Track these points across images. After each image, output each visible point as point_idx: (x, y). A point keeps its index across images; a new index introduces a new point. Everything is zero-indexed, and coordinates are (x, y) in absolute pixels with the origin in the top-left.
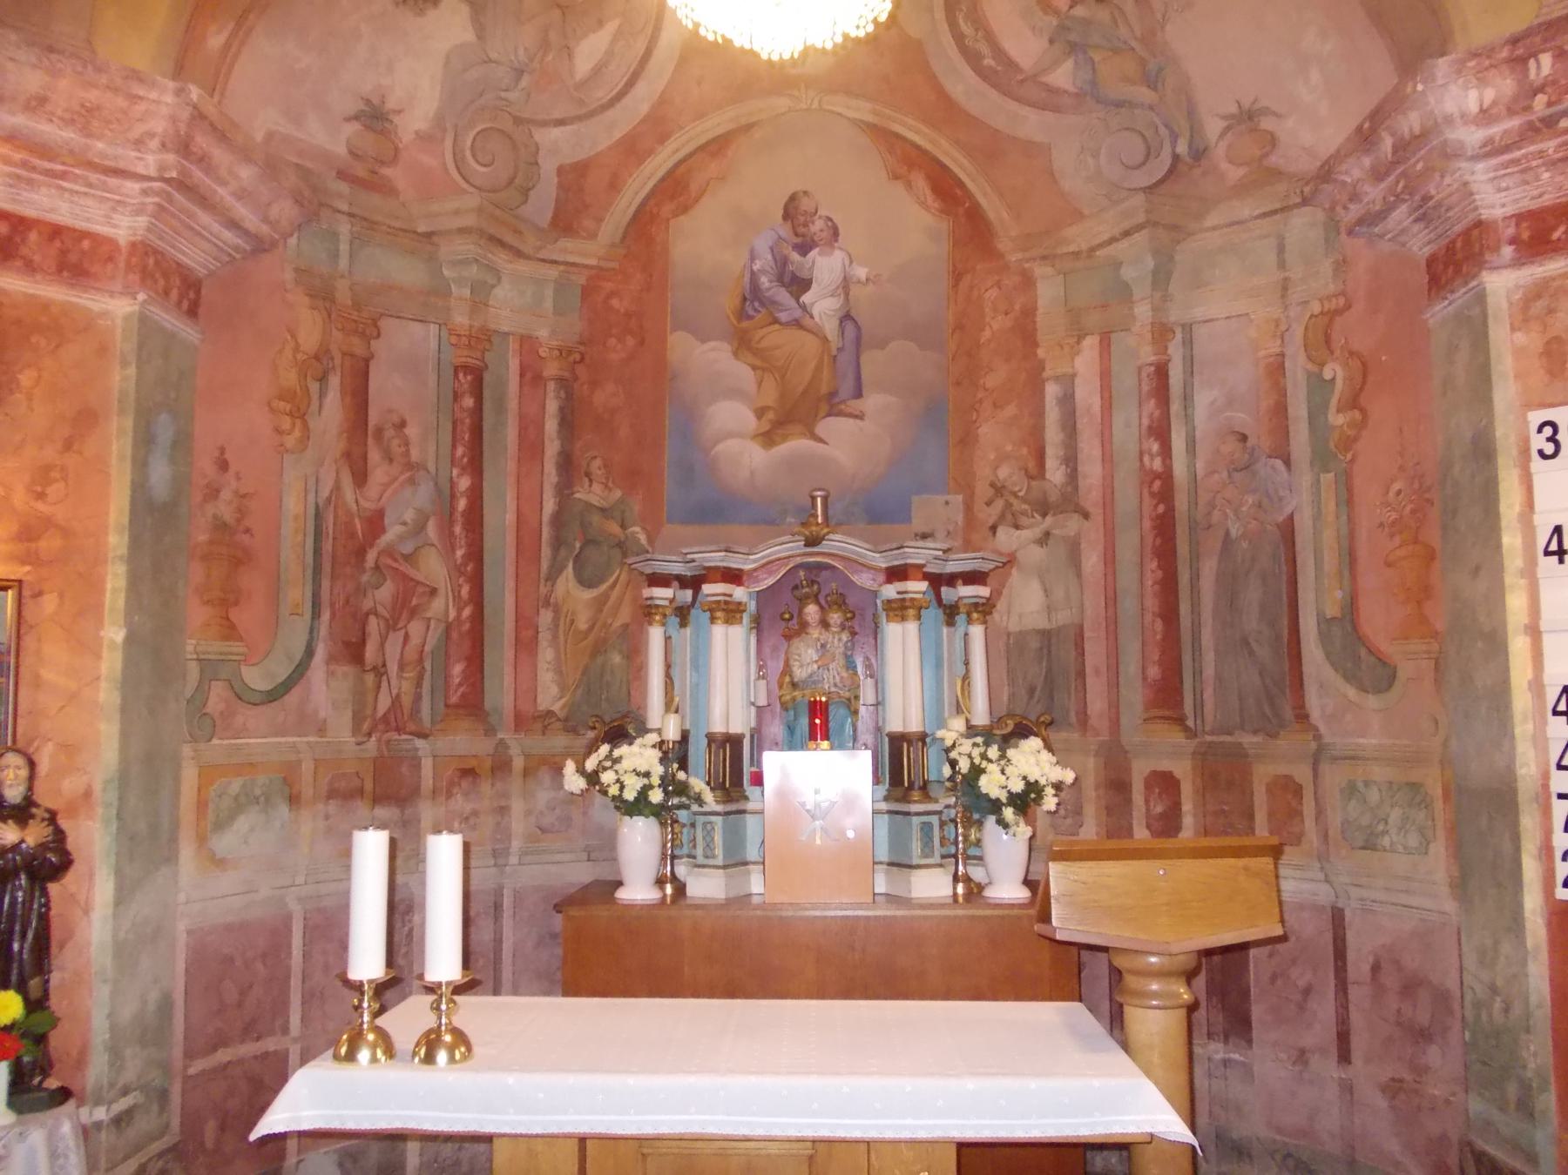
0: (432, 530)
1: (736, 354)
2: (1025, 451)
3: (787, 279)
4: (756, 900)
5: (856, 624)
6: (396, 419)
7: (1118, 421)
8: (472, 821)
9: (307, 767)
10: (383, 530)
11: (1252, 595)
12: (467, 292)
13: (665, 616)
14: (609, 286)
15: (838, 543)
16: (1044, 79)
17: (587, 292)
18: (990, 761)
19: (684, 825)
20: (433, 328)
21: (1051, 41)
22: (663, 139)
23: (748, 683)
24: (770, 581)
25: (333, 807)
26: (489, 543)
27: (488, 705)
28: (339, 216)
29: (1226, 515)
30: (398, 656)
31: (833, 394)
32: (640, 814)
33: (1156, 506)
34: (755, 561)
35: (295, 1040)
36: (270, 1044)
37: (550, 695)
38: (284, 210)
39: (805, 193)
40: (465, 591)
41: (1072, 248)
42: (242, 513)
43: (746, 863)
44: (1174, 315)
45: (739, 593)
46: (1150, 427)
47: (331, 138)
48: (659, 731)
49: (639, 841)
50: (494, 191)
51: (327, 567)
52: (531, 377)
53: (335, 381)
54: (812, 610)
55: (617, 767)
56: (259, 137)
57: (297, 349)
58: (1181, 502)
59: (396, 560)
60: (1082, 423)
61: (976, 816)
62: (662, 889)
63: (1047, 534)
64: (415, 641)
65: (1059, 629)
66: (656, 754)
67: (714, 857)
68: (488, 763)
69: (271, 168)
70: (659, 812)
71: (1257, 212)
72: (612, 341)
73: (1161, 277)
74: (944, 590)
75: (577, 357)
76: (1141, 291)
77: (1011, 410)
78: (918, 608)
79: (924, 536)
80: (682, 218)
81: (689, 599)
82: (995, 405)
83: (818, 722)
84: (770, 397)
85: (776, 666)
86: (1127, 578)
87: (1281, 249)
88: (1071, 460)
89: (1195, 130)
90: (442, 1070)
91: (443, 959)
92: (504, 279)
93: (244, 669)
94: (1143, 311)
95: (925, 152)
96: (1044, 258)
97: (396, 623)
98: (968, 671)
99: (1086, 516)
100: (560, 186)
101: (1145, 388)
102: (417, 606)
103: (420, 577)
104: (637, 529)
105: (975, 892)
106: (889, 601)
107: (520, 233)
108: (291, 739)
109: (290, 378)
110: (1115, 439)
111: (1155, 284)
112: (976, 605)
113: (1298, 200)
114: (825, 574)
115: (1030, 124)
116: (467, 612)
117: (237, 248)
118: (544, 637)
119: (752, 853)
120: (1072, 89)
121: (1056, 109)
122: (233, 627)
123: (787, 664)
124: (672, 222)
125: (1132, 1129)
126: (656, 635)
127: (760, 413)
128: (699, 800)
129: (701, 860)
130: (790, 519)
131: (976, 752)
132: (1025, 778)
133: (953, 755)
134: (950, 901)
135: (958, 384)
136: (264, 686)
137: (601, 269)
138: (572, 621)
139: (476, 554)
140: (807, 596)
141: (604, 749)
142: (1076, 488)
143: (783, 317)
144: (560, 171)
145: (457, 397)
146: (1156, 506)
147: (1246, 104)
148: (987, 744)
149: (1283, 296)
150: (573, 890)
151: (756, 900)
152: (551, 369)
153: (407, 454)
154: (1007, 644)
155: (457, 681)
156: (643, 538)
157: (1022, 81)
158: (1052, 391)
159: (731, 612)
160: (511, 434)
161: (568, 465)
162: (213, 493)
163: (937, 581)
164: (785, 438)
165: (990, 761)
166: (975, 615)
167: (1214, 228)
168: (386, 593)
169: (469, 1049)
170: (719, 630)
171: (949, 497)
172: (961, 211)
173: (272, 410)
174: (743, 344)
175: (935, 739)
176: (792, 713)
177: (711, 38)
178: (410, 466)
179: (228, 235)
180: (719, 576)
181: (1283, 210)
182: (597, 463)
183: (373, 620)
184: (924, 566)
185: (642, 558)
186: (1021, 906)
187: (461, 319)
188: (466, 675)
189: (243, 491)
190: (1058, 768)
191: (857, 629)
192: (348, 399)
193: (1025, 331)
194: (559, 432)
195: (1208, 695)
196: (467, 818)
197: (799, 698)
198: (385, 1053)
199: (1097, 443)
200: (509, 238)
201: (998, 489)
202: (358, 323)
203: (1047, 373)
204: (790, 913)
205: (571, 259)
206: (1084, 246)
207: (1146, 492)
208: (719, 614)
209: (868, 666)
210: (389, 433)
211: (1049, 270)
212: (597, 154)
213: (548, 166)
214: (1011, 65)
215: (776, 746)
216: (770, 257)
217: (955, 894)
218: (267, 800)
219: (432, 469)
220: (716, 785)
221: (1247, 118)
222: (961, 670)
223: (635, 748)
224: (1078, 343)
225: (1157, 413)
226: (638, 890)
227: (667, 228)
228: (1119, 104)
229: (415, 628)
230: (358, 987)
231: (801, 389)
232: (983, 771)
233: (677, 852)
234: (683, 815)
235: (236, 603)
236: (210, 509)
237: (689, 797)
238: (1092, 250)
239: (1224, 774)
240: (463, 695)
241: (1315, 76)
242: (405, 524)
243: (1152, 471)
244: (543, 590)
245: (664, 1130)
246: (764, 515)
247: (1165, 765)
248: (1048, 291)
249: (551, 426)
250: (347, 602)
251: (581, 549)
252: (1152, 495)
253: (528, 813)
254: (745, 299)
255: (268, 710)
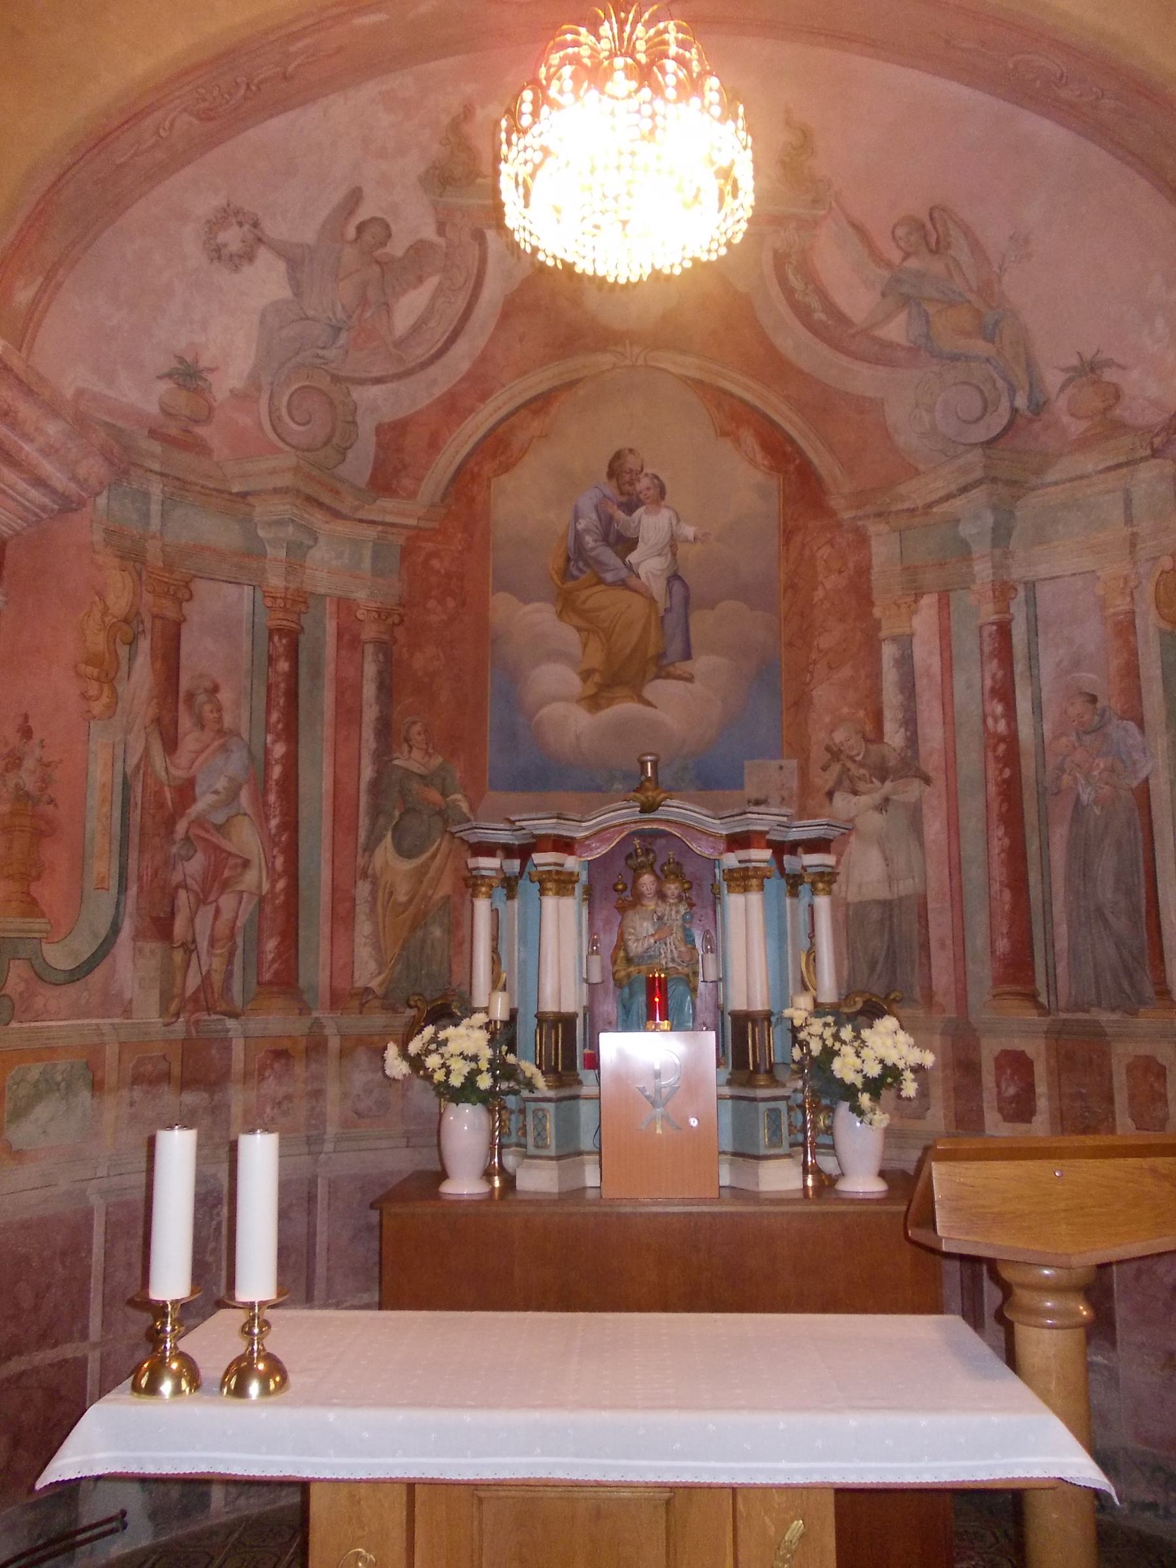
0: (244, 797)
1: (560, 615)
2: (861, 713)
3: (612, 538)
4: (591, 1194)
5: (693, 894)
6: (208, 684)
7: (959, 681)
8: (284, 1107)
9: (111, 1052)
10: (194, 800)
11: (1106, 864)
12: (282, 554)
13: (491, 887)
14: (429, 546)
15: (678, 810)
16: (877, 333)
17: (406, 553)
18: (844, 1042)
19: (512, 1112)
20: (248, 590)
21: (883, 295)
22: (484, 397)
23: (580, 957)
24: (604, 850)
25: (138, 1093)
26: (305, 812)
27: (302, 983)
28: (151, 476)
29: (1075, 779)
30: (208, 933)
31: (661, 655)
32: (467, 1101)
33: (1001, 771)
34: (587, 828)
35: (94, 1346)
36: (69, 1351)
37: (367, 971)
38: (93, 468)
39: (631, 451)
40: (279, 862)
41: (907, 505)
42: (45, 782)
43: (580, 1153)
44: (1017, 573)
45: (571, 863)
46: (993, 691)
47: (142, 396)
48: (486, 1010)
49: (466, 1127)
50: (308, 450)
51: (135, 837)
52: (349, 640)
53: (144, 644)
54: (647, 881)
55: (442, 1050)
56: (69, 394)
57: (105, 611)
58: (1028, 767)
59: (207, 831)
60: (921, 683)
61: (825, 1102)
62: (490, 1182)
63: (887, 800)
64: (226, 915)
65: (901, 899)
66: (482, 1037)
67: (546, 1147)
68: (302, 1045)
69: (81, 424)
70: (488, 1099)
71: (1100, 467)
72: (432, 604)
73: (1001, 535)
74: (786, 858)
75: (396, 619)
76: (981, 548)
77: (846, 672)
78: (762, 876)
79: (758, 803)
80: (504, 477)
81: (517, 869)
82: (830, 668)
83: (654, 999)
84: (595, 658)
85: (609, 940)
86: (972, 847)
87: (1128, 503)
88: (910, 722)
89: (1034, 383)
90: (254, 1404)
91: (257, 1277)
92: (322, 540)
93: (45, 947)
94: (983, 570)
95: (754, 409)
96: (879, 515)
97: (206, 898)
98: (813, 944)
99: (927, 780)
100: (379, 445)
101: (987, 649)
102: (229, 878)
103: (233, 850)
104: (458, 796)
105: (826, 1184)
106: (730, 871)
107: (337, 493)
108: (94, 1021)
109: (98, 642)
110: (957, 700)
111: (995, 543)
112: (822, 874)
113: (1149, 452)
114: (661, 842)
115: (864, 379)
116: (281, 884)
117: (43, 508)
118: (362, 910)
119: (587, 1142)
120: (903, 341)
121: (890, 363)
122: (34, 902)
123: (621, 937)
124: (494, 481)
125: (1037, 1473)
126: (482, 907)
127: (586, 675)
128: (530, 1085)
129: (531, 1150)
130: (617, 786)
131: (828, 1033)
132: (882, 1061)
133: (802, 1035)
134: (800, 1195)
135: (790, 644)
136: (66, 964)
137: (420, 529)
138: (391, 894)
139: (291, 824)
140: (642, 866)
141: (429, 1031)
142: (916, 752)
143: (609, 577)
144: (379, 430)
145: (271, 660)
146: (1001, 771)
147: (1088, 356)
148: (839, 1024)
149: (1131, 553)
150: (395, 1181)
151: (591, 1194)
152: (370, 632)
153: (220, 720)
154: (847, 916)
155: (270, 957)
156: (464, 806)
157: (853, 336)
158: (889, 651)
159: (563, 883)
160: (328, 697)
161: (385, 729)
162: (15, 761)
163: (780, 849)
164: (610, 702)
165: (844, 1042)
166: (820, 886)
167: (1056, 483)
168: (196, 865)
169: (284, 1379)
170: (550, 902)
171: (784, 762)
172: (791, 468)
173: (78, 675)
174: (567, 605)
175: (781, 1018)
176: (627, 990)
177: (550, 263)
178: (221, 732)
179: (34, 494)
180: (550, 845)
181: (1127, 464)
182: (417, 728)
183: (182, 894)
184: (767, 832)
185: (466, 826)
186: (878, 1201)
187: (276, 581)
188: (279, 954)
189: (45, 760)
190: (917, 1051)
191: (694, 900)
192: (158, 665)
193: (861, 590)
194: (378, 697)
195: (1061, 969)
196: (280, 1103)
197: (635, 974)
198: (190, 1384)
199: (936, 704)
200: (327, 499)
201: (835, 753)
202: (170, 587)
203: (883, 634)
204: (628, 1210)
205: (389, 519)
206: (920, 503)
207: (990, 754)
208: (549, 885)
209: (707, 940)
210: (201, 698)
211: (883, 527)
212: (418, 413)
213: (366, 426)
214: (842, 319)
215: (611, 1027)
216: (594, 516)
217: (805, 1187)
218: (68, 1087)
219: (245, 736)
220: (549, 1071)
221: (1089, 370)
222: (805, 943)
223: (461, 1030)
224: (915, 601)
225: (1000, 674)
226: (464, 1185)
227: (489, 487)
228: (955, 358)
229: (227, 902)
230: (159, 1310)
231: (628, 650)
232: (837, 1053)
233: (504, 1141)
234: (511, 1101)
235: (38, 877)
236: (12, 779)
237: (518, 1082)
238: (930, 506)
239: (1080, 1054)
240: (276, 973)
241: (1160, 324)
242: (216, 792)
243: (995, 734)
244: (361, 861)
245: (505, 1475)
246: (584, 780)
247: (1018, 1044)
248: (883, 550)
249: (369, 691)
250: (156, 873)
251: (401, 816)
252: (997, 759)
253: (345, 1096)
254: (568, 560)
255: (71, 991)
